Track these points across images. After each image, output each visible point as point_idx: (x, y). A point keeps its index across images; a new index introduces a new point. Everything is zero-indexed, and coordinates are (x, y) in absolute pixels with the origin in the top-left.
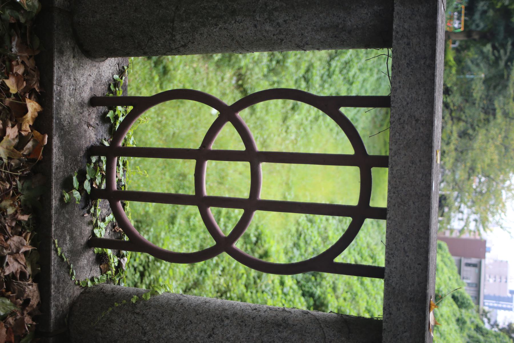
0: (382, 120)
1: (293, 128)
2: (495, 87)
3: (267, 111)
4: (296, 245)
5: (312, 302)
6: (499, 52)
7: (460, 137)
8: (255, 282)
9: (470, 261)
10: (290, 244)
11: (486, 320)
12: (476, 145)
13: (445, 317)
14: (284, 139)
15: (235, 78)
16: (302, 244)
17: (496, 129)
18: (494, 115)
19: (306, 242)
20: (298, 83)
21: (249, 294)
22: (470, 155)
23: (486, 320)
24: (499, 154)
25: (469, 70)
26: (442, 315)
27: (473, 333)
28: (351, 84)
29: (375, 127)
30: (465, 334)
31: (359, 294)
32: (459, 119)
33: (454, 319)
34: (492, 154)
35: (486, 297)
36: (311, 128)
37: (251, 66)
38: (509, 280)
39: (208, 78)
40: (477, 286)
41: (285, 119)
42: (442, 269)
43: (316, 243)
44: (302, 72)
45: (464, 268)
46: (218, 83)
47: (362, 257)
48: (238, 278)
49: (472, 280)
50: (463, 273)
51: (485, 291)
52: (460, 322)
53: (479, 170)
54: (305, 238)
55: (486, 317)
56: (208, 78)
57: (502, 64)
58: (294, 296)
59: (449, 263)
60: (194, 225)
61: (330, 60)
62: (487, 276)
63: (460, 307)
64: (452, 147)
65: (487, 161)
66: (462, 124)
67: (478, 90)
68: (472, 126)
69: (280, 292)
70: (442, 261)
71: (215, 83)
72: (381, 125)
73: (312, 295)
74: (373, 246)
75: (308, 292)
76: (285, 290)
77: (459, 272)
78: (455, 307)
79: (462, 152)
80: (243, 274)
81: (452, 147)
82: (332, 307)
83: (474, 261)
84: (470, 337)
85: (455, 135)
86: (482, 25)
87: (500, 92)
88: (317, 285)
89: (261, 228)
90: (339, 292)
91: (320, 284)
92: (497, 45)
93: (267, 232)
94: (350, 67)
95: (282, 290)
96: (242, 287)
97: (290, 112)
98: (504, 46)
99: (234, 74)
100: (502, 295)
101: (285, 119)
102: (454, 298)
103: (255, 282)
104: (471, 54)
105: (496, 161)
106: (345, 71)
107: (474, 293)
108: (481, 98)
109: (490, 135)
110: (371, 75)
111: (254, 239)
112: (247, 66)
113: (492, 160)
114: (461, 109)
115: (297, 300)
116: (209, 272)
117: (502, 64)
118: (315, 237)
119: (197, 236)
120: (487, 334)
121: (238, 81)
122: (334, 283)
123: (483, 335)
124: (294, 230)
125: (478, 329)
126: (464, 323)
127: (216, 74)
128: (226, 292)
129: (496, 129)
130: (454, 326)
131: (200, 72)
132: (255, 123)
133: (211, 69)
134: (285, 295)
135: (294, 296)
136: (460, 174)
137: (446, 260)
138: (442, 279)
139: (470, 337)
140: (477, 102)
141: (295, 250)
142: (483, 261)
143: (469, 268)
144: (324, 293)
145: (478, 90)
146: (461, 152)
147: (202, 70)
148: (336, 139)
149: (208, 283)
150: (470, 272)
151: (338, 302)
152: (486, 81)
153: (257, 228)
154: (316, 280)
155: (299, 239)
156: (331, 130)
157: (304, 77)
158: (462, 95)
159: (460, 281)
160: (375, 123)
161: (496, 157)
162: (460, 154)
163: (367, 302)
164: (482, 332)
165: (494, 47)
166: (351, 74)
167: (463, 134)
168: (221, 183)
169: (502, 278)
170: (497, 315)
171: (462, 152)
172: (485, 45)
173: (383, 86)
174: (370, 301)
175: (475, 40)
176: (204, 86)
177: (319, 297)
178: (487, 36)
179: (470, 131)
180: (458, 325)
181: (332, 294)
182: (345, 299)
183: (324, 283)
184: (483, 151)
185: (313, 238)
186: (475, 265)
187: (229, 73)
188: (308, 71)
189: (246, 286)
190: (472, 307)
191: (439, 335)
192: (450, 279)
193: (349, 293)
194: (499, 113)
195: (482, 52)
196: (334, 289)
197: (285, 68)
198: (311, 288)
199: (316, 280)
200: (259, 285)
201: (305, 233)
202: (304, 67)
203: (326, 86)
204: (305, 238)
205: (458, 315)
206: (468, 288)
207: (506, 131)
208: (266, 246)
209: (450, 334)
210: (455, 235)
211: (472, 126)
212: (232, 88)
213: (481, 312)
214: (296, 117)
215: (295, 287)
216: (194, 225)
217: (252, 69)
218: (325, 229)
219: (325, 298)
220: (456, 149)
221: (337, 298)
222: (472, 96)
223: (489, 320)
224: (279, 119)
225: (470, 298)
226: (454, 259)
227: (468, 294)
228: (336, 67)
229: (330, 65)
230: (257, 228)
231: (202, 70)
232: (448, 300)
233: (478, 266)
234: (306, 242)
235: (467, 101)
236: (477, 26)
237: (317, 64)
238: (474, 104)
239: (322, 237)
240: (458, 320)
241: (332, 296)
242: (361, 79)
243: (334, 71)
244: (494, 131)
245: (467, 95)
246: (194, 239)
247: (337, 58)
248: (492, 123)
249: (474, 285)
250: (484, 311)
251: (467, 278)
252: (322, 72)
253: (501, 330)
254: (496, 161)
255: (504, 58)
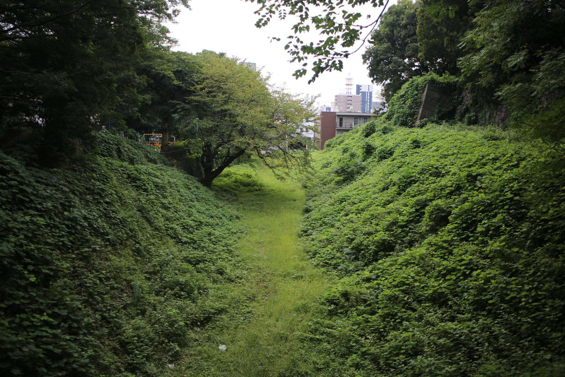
0: (231, 195)
1: (238, 272)
2: (205, 111)
3: (223, 298)
4: (335, 267)
5: (382, 253)
6: (178, 109)
7: (243, 135)
8: (369, 305)
9: (338, 124)
10: (334, 272)
11: (381, 112)
12: (249, 123)
13: (382, 142)
14: (247, 280)
15: (195, 328)
16: (335, 262)
17: (237, 109)
18: (226, 110)
19: (332, 258)
20: (200, 270)
21: (380, 311)
22: (256, 127)
23: (381, 112)
24: (256, 106)
25: (193, 128)
26: (382, 145)
27: (393, 121)
28: (201, 223)
29: (237, 200)
30: (394, 127)
31: (372, 213)
32: (230, 136)
33: (384, 136)
34: (256, 112)
35: (363, 110)
36: (238, 256)
37: (185, 316)
38: (350, 95)
39: (195, 355)
40: (356, 117)
41: (231, 280)
42: (346, 144)
43: (332, 250)
44: (190, 267)
45: (344, 127)
46: (200, 345)
47: (342, 210)
48: (367, 321)
49: (352, 121)
50: (348, 127)
51: (359, 112)
52: (385, 131)
53: (269, 121)
54: (329, 260)
55: (379, 111)
56: (195, 355)
57: (187, 106)
58: (379, 269)
59: (341, 139)
60: (324, 364)
61: (182, 242)
62: (348, 110)
63: (374, 131)
64: (251, 141)
65: (262, 115)
66: (234, 133)
67: (207, 123)
68: (234, 126)
69: (375, 282)
70: (339, 144)
71: (200, 348)
72: (235, 195)
73: (376, 253)
74: (332, 201)
75: (373, 256)
76: (374, 277)
77: (348, 131)
78: (374, 135)
79: (255, 134)
80: (363, 317)
81: (251, 141)
82: (384, 236)
83: (338, 120)
84: (395, 124)
85: (242, 139)
86: (159, 120)
87: (208, 107)
88: (367, 249)
89: (323, 300)
90: (372, 230)
91: (367, 246)
92: (173, 110)
93: (326, 295)
94: (187, 225)
95: (374, 280)
96: (374, 317)
97: (225, 276)
98: (174, 105)
99: (192, 329)
100: (361, 99)
101: (231, 280)
102: (367, 136)
103: (369, 305)
104: (180, 127)
105: (262, 109)
106: (191, 229)
107: (362, 120)
108: (213, 121)
109: (242, 113)
110: (194, 206)
111: (333, 306)
112: (185, 319)
113: (261, 112)
114: (222, 135)
115: (380, 266)
116: (364, 349)
117: (187, 106)
118: (328, 251)
119: (333, 361)
120: (392, 111)
121: (198, 326)
122: (364, 234)
123: (393, 114)
124: (323, 269)
125: (389, 118)
126: (385, 128)
127: (192, 347)
128: (380, 333)
129: (237, 109)
130: (388, 136)
131: (190, 363)
132: (234, 308)
133: (187, 352)
134: (378, 277)
135: (379, 269)
136: (272, 134)
137: (338, 141)
138: (354, 144)
139: (395, 124)
140: (216, 124)
141: (339, 268)
142: (337, 114)
143: (343, 124)
144: (374, 243)
145: (207, 123)
146: (255, 134)
147: (187, 360)
148: (247, 234)
149: (373, 350)
150: (347, 123)
151: (380, 231)
152: (201, 118)
153: (323, 304)
154: (363, 250)
155: (330, 265)
156: (239, 238)
157: (194, 265)
158: (211, 135)
159: (354, 130)
160: (233, 200)
161: (258, 109)
162: (257, 135)
163: (377, 205)
164: (391, 115)
165: (174, 112)
166: (191, 223)
167: (242, 133)
168: (286, 339)
169: (348, 99)
170: (376, 103)
171: (255, 134)
172: (173, 118)
173: (204, 196)
174: (377, 203)
175: (169, 126)
176: (202, 359)
177: (377, 247)
178: (167, 118)
179: (239, 128)
180: (388, 133)
181: (374, 235)
182: (377, 225)
183: (365, 243)
184: (253, 117)
185: (328, 252)
186: (341, 120)
187: (191, 334)
188: (189, 262)
189: (373, 313)
190: (373, 122)
191: (397, 148)
192: (353, 139)
193: (372, 221)
194: (226, 107)
195: (179, 120)
196: (370, 234)
197: (186, 284)
198: (370, 254)
199: (363, 250)
200: (372, 301)
201: (325, 260)
202: (185, 265)
203: (203, 245)
204: (329, 260)
205: (380, 133)
206: (359, 124)
207: (238, 102)
208: (338, 295)
209: (396, 139)
210: (319, 136)
211: (234, 126)
212: (204, 331)
213: (376, 115)
214: (228, 271)
215: (370, 267)
216: (324, 364)
217: (188, 314)
218: (320, 241)
219: (378, 242)
220: (253, 139)
221: (377, 231)
222: (212, 128)
223: (380, 109)
224: (231, 286)
225: (366, 124)
226: (337, 135)
227: (363, 126)
228: (187, 237)
229: (186, 243)
230: (323, 304)
231: (187, 360)
232: (369, 140)
233: (341, 117)
234: (332, 258)
235: (216, 131)
236: (159, 123)
237: (184, 254)
238: (217, 125)
239: (328, 244)
240: (384, 133)
241: (376, 236)
242: (197, 215)
243: (190, 239)
244: (238, 111)
245: (211, 131)
246: (336, 364)
247: (180, 237)
248: (233, 112)
249: (356, 120)
250: (374, 113)
251: (351, 125)
252: (191, 249)
253: (388, 101)
254: (262, 109)
255: (183, 105)
